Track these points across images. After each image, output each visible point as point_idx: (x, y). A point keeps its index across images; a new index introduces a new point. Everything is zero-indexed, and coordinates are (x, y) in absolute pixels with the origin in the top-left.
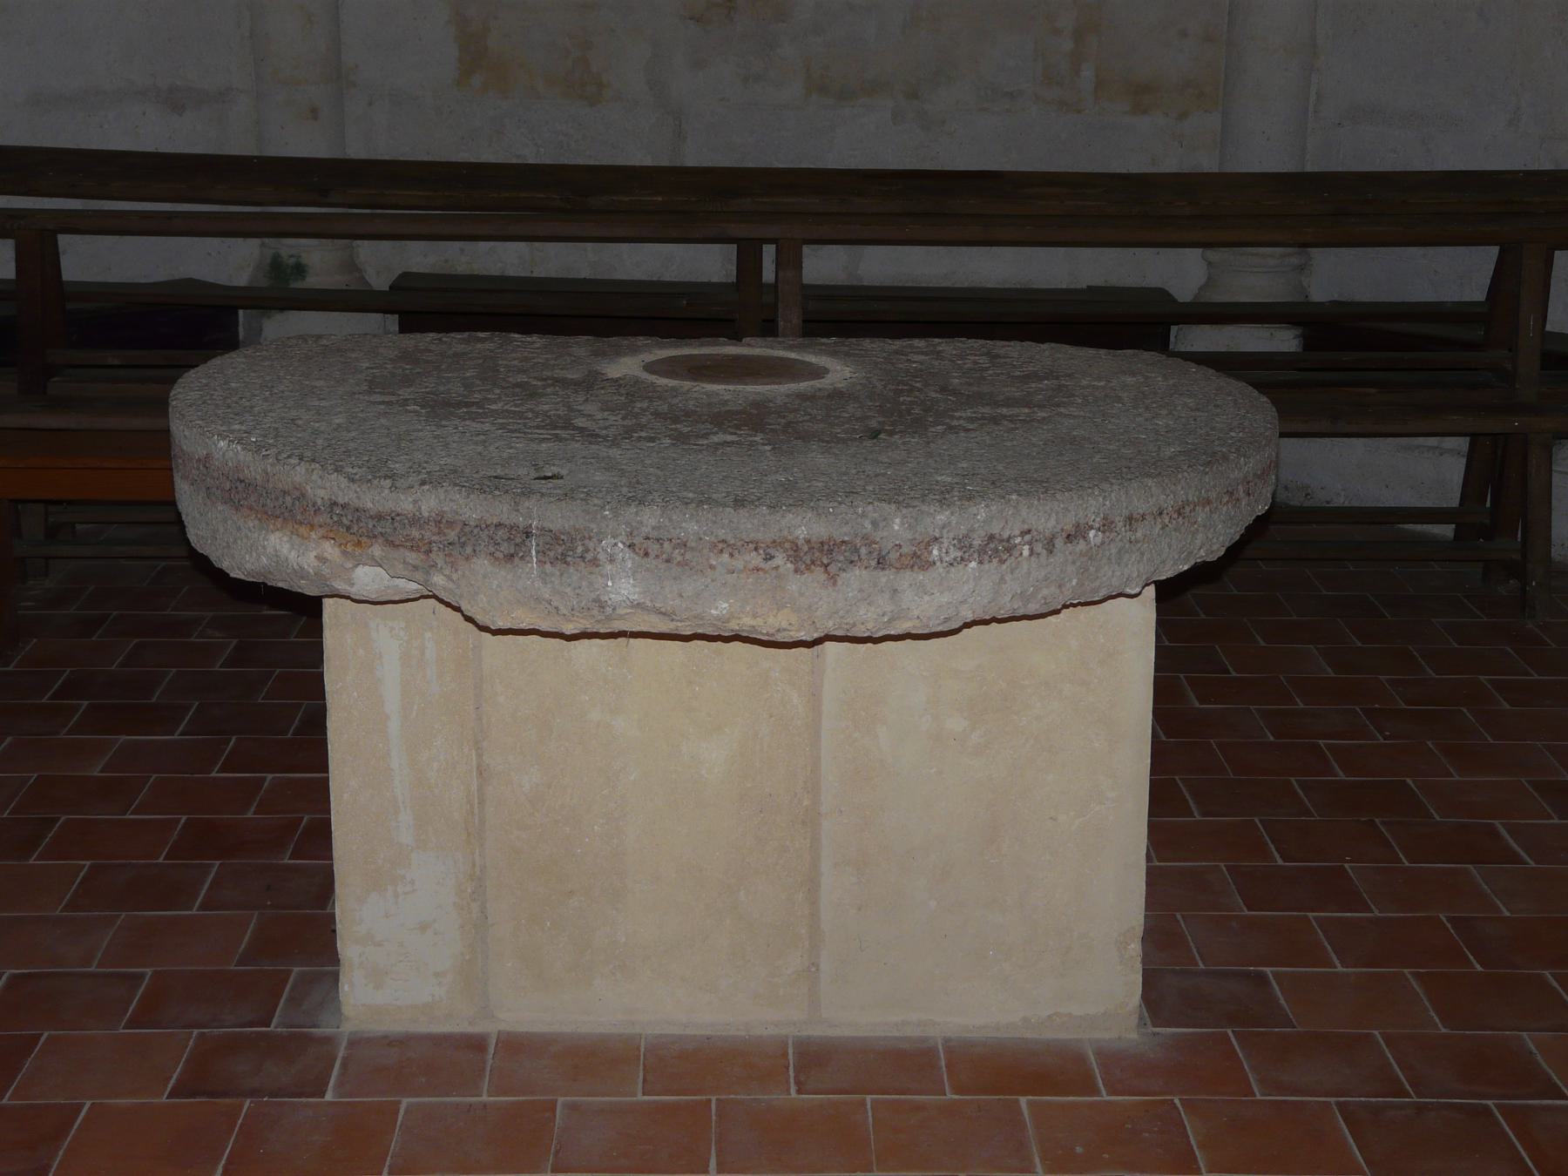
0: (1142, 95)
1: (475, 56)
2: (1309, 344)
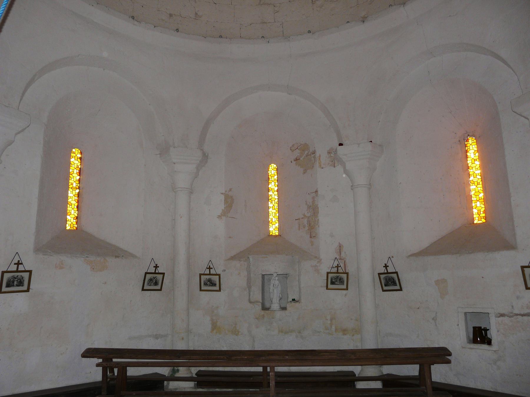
0: (345, 331)
1: (215, 327)
2: (384, 385)
